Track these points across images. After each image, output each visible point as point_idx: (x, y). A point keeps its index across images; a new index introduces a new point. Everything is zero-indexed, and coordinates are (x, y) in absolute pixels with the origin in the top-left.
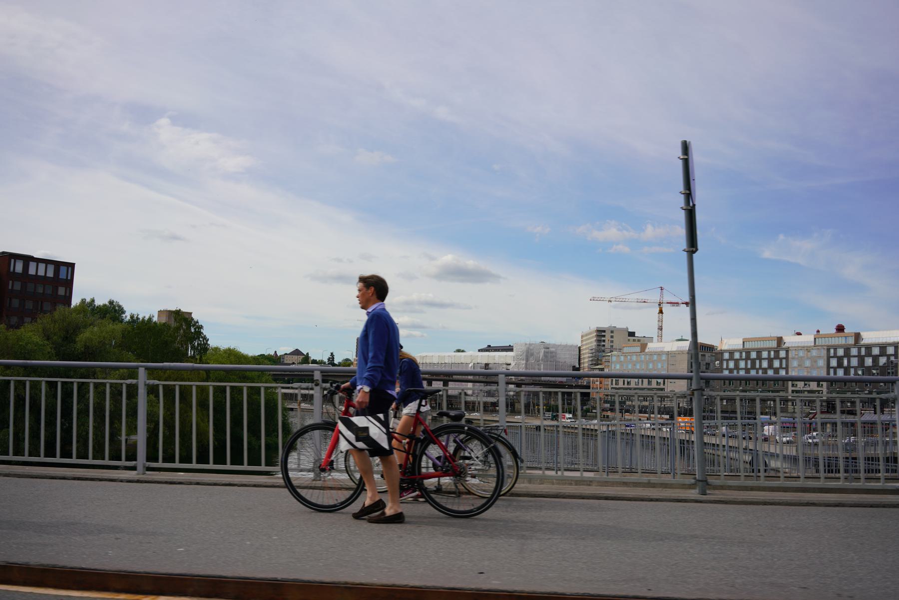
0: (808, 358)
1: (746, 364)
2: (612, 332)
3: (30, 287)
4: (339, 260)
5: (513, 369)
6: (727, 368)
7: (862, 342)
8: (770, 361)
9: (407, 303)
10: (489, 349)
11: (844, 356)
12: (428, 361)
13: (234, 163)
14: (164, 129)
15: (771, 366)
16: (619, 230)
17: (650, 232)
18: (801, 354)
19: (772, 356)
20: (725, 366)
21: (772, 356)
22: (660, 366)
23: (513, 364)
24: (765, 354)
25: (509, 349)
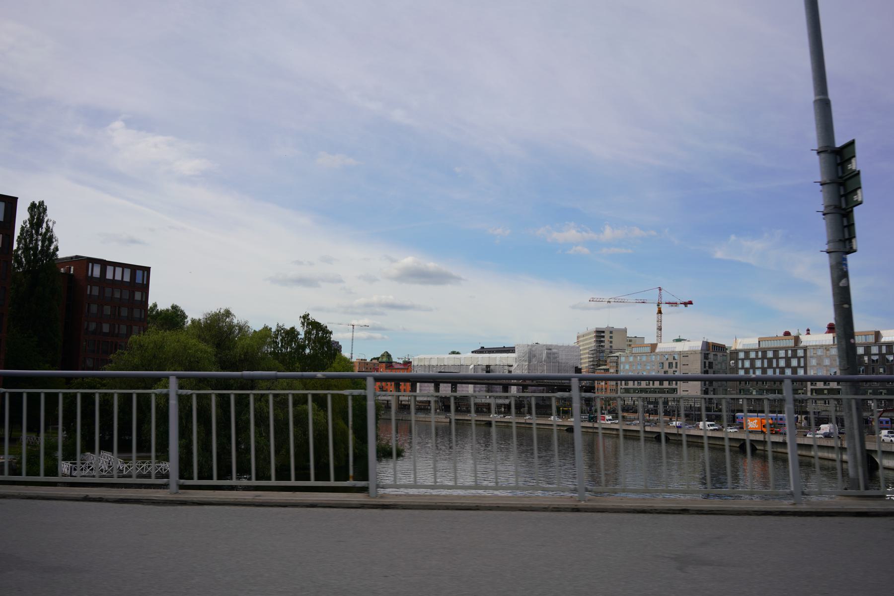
0: (827, 357)
1: (763, 363)
2: (611, 332)
3: (108, 292)
4: (299, 263)
5: (517, 371)
6: (743, 368)
7: (883, 340)
8: (788, 360)
9: (367, 305)
10: (482, 350)
11: (865, 354)
12: (427, 363)
13: (189, 166)
14: (118, 133)
15: (788, 365)
16: (578, 231)
17: (608, 233)
18: (819, 352)
19: (790, 355)
20: (740, 366)
21: (790, 355)
22: (627, 367)
23: (515, 365)
24: (782, 353)
25: (511, 350)
